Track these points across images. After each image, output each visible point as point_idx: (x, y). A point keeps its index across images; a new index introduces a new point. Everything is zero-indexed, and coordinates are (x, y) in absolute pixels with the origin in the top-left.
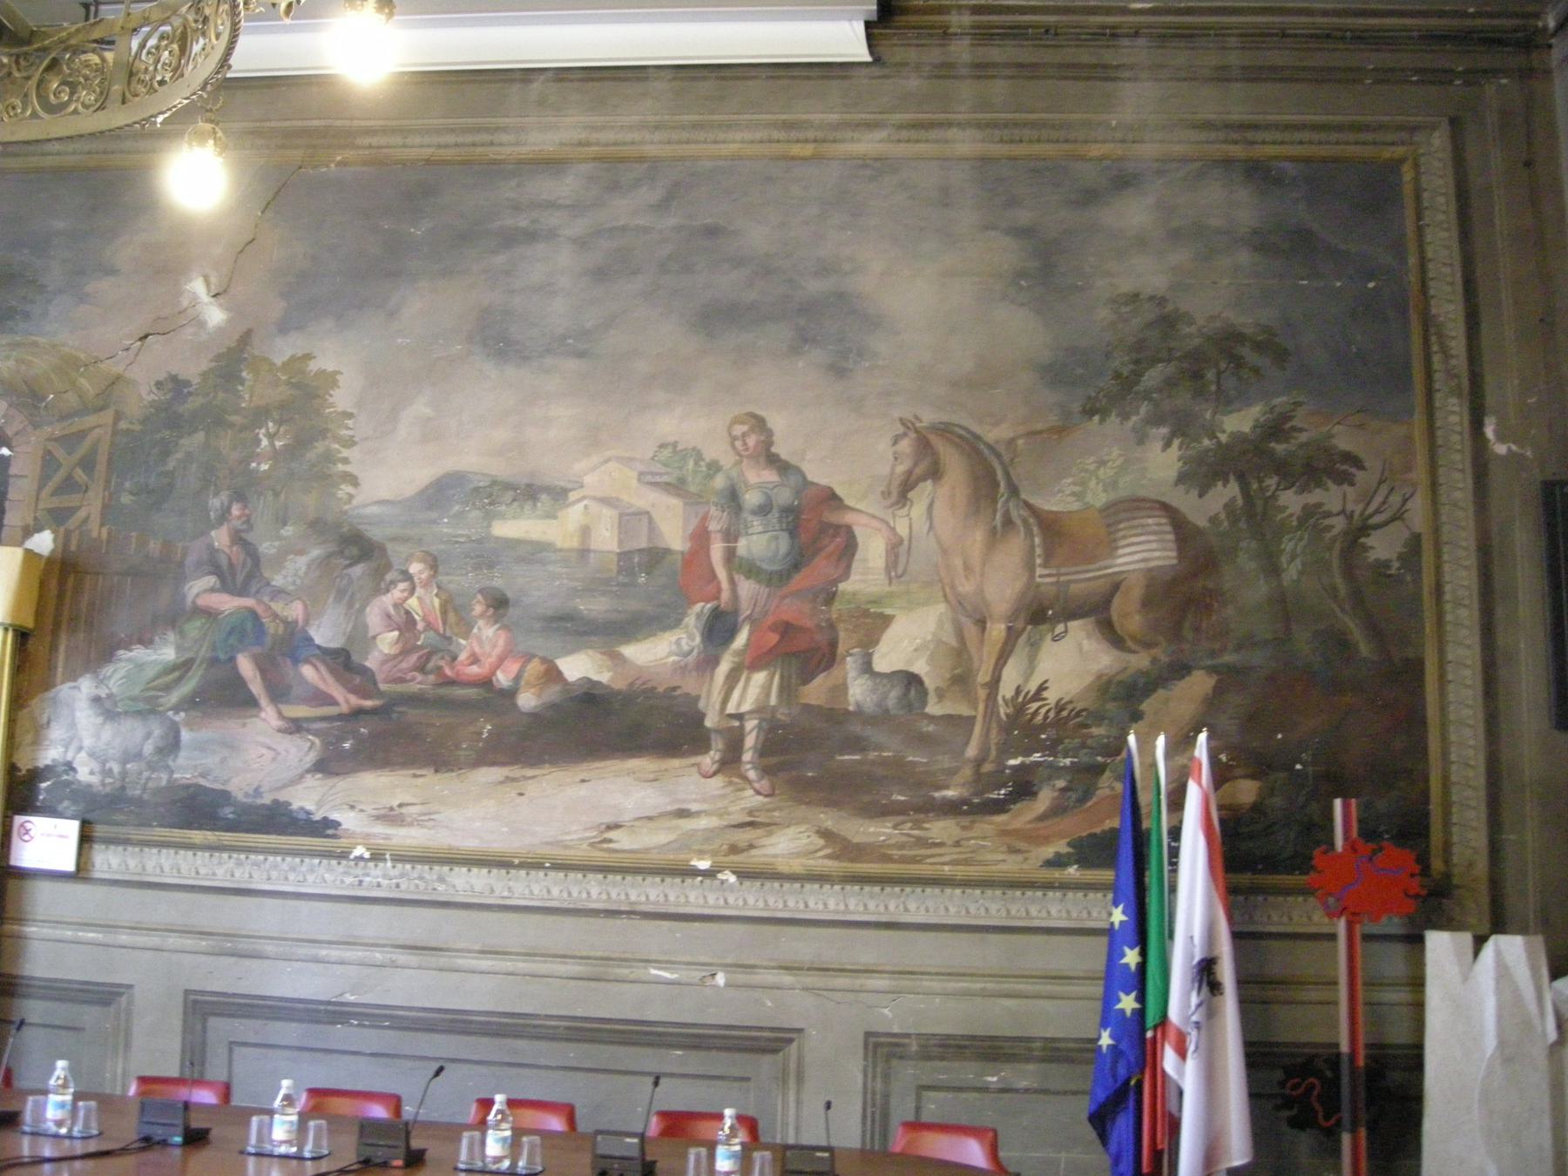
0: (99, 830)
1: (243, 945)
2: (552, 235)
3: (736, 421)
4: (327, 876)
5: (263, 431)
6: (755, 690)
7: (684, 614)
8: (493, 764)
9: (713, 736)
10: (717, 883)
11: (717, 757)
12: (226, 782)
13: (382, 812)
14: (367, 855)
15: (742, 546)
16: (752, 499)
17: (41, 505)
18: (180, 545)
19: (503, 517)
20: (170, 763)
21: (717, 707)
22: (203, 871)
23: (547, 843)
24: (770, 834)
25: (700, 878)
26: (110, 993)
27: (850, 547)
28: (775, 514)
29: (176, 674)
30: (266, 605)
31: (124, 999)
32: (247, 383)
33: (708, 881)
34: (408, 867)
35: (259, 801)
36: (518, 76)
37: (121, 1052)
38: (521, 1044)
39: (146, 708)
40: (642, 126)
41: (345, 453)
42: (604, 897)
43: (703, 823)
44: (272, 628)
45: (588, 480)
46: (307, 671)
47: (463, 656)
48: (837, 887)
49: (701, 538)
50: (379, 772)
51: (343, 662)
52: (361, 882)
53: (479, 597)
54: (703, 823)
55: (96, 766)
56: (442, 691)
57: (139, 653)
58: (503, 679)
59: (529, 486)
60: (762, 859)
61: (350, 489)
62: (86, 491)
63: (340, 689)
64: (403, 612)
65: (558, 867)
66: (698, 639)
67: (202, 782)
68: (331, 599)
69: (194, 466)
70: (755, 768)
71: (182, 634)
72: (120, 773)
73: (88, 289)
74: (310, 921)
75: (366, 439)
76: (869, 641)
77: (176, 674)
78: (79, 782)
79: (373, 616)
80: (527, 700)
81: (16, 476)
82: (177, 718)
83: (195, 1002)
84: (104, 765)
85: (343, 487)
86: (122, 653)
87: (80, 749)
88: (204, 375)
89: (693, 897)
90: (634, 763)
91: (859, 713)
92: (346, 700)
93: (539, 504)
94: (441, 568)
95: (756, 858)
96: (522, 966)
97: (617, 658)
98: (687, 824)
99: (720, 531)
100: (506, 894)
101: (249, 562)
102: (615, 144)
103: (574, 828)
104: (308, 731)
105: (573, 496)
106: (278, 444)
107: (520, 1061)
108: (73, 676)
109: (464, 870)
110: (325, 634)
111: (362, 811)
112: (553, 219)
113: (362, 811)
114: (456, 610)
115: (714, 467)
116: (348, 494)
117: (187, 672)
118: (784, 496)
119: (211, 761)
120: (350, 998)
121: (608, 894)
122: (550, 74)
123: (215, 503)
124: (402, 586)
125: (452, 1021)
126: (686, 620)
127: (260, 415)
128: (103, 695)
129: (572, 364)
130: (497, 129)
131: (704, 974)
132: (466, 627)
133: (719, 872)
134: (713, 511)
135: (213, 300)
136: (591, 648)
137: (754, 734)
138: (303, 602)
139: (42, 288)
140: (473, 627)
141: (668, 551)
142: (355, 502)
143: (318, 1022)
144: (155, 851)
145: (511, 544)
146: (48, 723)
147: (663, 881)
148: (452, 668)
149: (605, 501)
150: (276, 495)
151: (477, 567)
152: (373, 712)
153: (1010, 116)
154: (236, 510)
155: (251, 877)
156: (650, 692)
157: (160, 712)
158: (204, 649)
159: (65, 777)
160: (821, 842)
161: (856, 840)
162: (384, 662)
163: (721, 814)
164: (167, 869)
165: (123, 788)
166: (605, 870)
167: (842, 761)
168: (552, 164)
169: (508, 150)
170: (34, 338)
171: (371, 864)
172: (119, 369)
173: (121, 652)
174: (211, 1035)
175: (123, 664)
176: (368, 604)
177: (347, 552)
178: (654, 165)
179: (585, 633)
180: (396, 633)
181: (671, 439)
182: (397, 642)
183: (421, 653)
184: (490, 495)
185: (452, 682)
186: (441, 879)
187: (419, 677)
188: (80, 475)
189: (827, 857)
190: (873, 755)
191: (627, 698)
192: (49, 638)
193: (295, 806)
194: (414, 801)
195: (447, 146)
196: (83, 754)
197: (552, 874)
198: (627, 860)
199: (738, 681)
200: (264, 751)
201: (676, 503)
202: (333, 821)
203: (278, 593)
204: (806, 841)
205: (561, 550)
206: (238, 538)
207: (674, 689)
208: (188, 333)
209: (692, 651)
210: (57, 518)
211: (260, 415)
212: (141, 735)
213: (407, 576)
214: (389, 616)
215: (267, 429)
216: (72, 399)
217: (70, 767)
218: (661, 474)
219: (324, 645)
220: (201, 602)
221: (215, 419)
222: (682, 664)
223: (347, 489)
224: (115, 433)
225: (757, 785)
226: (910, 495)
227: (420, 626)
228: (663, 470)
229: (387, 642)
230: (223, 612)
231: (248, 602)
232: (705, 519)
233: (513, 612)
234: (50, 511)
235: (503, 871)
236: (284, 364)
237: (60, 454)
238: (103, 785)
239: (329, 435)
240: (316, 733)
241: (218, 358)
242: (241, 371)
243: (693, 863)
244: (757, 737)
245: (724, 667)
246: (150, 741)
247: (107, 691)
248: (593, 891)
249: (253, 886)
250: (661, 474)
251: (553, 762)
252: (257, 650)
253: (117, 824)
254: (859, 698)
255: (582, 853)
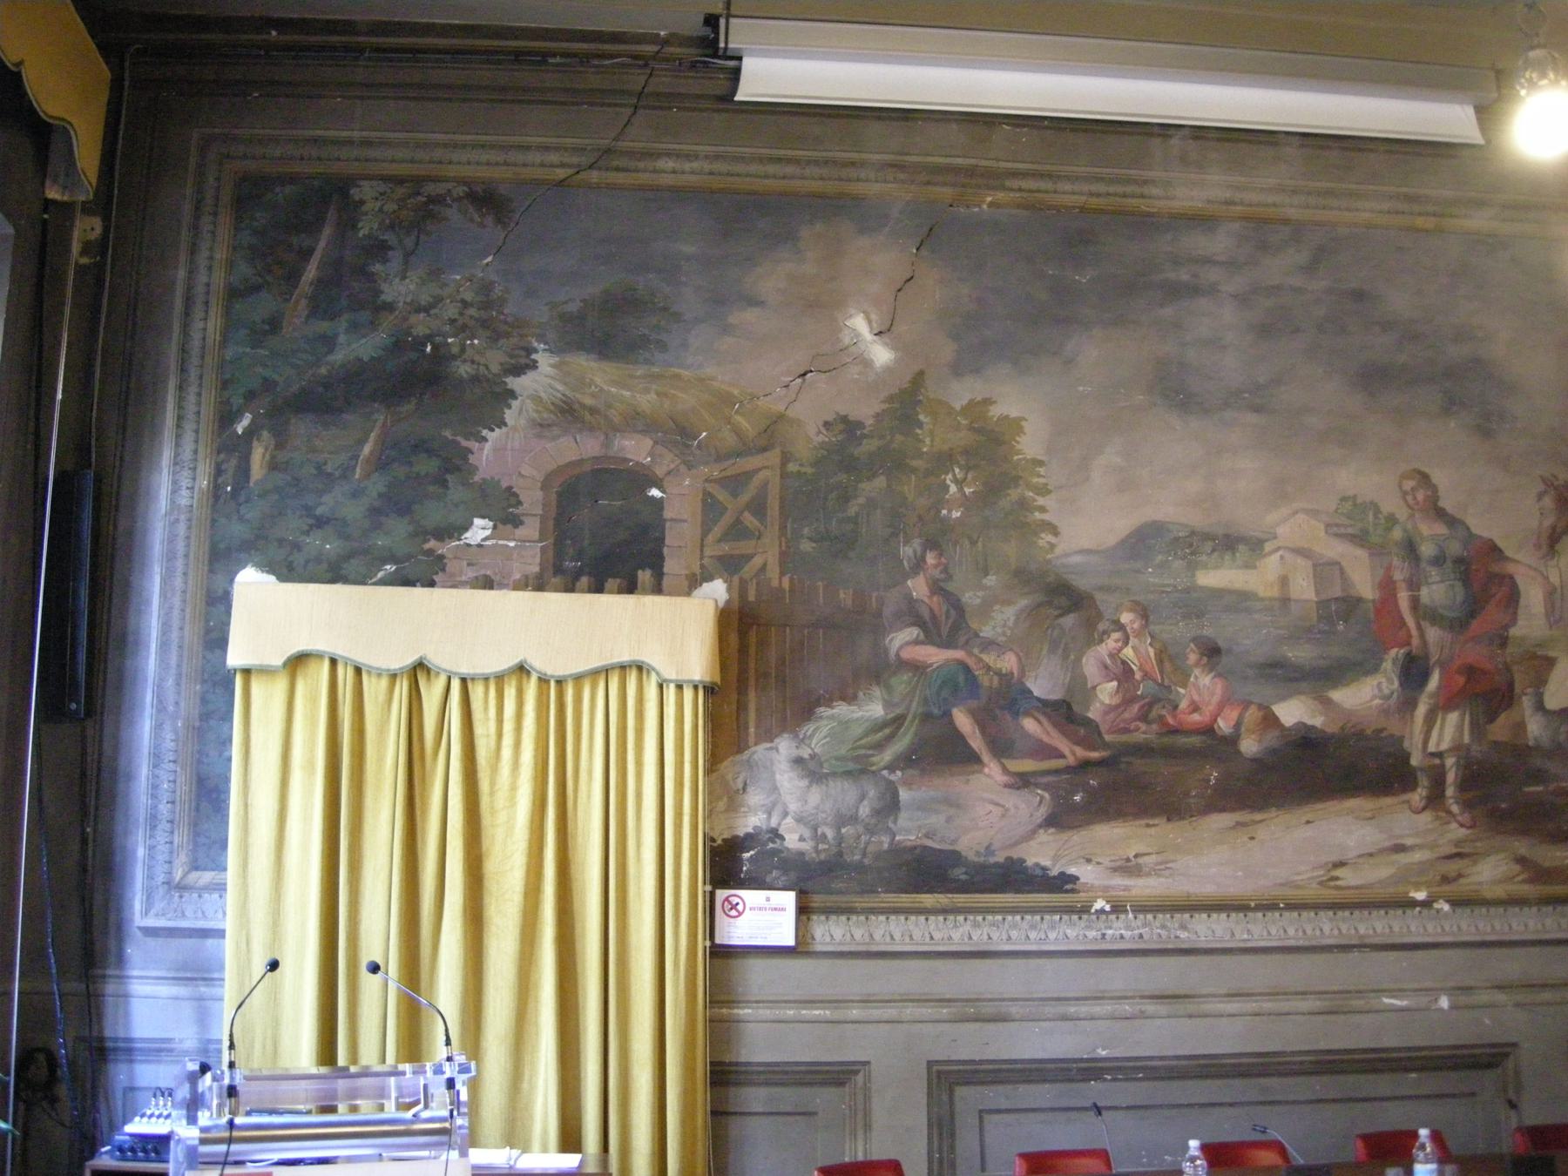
0: (817, 900)
1: (988, 1009)
2: (1212, 290)
3: (1404, 476)
4: (1069, 932)
5: (950, 476)
6: (1450, 730)
7: (1382, 660)
8: (1223, 810)
9: (1419, 773)
10: (1433, 912)
11: (1424, 794)
12: (954, 842)
13: (1118, 864)
14: (1108, 908)
15: (1424, 593)
16: (1427, 550)
17: (708, 552)
18: (874, 594)
19: (1205, 567)
20: (891, 825)
21: (1420, 746)
22: (937, 936)
23: (1281, 885)
24: (1475, 863)
25: (1418, 909)
26: (843, 1072)
27: (1513, 598)
28: (1449, 564)
29: (887, 731)
30: (976, 656)
31: (860, 1078)
32: (926, 427)
33: (1425, 912)
34: (1150, 916)
35: (992, 860)
36: (1156, 130)
37: (860, 1133)
38: (1273, 1082)
39: (858, 769)
40: (1281, 189)
41: (1041, 501)
42: (1336, 932)
43: (1417, 856)
44: (985, 680)
45: (1280, 531)
46: (1029, 724)
47: (1183, 705)
48: (1534, 909)
49: (1387, 586)
50: (1113, 824)
51: (1064, 713)
52: (1104, 935)
53: (1192, 645)
54: (1417, 856)
55: (807, 833)
56: (1166, 740)
57: (841, 709)
58: (1224, 726)
59: (1227, 536)
60: (1472, 887)
61: (1050, 538)
62: (759, 538)
63: (1065, 741)
64: (1119, 662)
65: (1292, 907)
66: (1396, 684)
67: (929, 843)
68: (1044, 652)
69: (879, 511)
70: (1457, 803)
71: (889, 688)
72: (834, 839)
73: (732, 320)
74: (1051, 978)
75: (1061, 487)
76: (1540, 682)
77: (887, 731)
78: (788, 849)
79: (1090, 666)
80: (1249, 746)
81: (672, 520)
82: (892, 777)
83: (939, 1072)
84: (816, 830)
85: (1043, 535)
86: (822, 711)
87: (785, 814)
88: (878, 417)
89: (1410, 927)
90: (1352, 803)
91: (1538, 748)
92: (1072, 753)
93: (1238, 555)
94: (1151, 617)
95: (1463, 887)
96: (1268, 1006)
97: (1327, 703)
98: (1404, 859)
99: (1404, 580)
100: (1245, 936)
101: (953, 612)
102: (1257, 205)
103: (1303, 868)
104: (1037, 785)
105: (1268, 547)
106: (967, 491)
107: (1271, 1098)
108: (768, 736)
109: (1204, 916)
110: (1042, 685)
111: (1098, 863)
112: (1212, 275)
113: (1098, 863)
114: (1171, 659)
115: (1392, 520)
116: (1048, 542)
117: (898, 728)
118: (1455, 548)
119: (936, 820)
120: (1103, 1053)
121: (1339, 930)
122: (1186, 132)
123: (907, 551)
124: (1116, 635)
125: (1206, 1066)
126: (1384, 664)
127: (944, 460)
128: (806, 756)
129: (1252, 418)
130: (1145, 182)
131: (1430, 998)
132: (1184, 679)
133: (1433, 902)
134: (1396, 562)
135: (875, 338)
136: (1300, 693)
137: (1454, 769)
138: (1017, 655)
139: (677, 317)
140: (1190, 676)
141: (1360, 600)
142: (1058, 551)
143: (1071, 1080)
144: (882, 918)
145: (1218, 593)
146: (744, 789)
147: (1386, 913)
148: (1174, 717)
149: (1299, 552)
150: (973, 543)
151: (1186, 616)
152: (1100, 763)
153: (768, 151)
154: (931, 559)
155: (990, 938)
156: (1360, 735)
157: (873, 772)
158: (914, 704)
159: (771, 845)
160: (1517, 868)
161: (1547, 864)
162: (1106, 713)
163: (1432, 846)
164: (897, 936)
165: (840, 854)
166: (1335, 906)
167: (1529, 793)
168: (1202, 221)
169: (1162, 203)
170: (677, 371)
171: (1113, 917)
172: (781, 408)
173: (822, 709)
174: (959, 1105)
175: (825, 722)
176: (1082, 656)
177: (1056, 602)
178: (1297, 230)
179: (1296, 680)
180: (1115, 684)
181: (1351, 493)
182: (1117, 692)
183: (1142, 702)
184: (1191, 545)
185: (1175, 731)
186: (1183, 927)
187: (1143, 727)
188: (750, 520)
189: (1523, 881)
190: (1552, 787)
191: (1341, 739)
192: (734, 697)
193: (1030, 862)
194: (1150, 850)
195: (1098, 195)
196: (789, 820)
197: (1287, 914)
198: (1351, 896)
199: (1435, 722)
200: (991, 807)
201: (1361, 553)
202: (1072, 876)
203: (988, 645)
204: (1505, 868)
205: (1262, 599)
206: (937, 588)
207: (1381, 730)
208: (854, 372)
209: (1392, 693)
210: (729, 566)
211: (944, 460)
212: (859, 799)
213: (1120, 627)
214: (1106, 667)
215: (954, 475)
216: (729, 439)
217: (775, 834)
218: (1346, 526)
219: (1043, 697)
220: (905, 655)
221: (893, 463)
222: (1385, 706)
223: (1047, 537)
224: (784, 475)
225: (1460, 818)
226: (1557, 547)
227: (1138, 676)
228: (1347, 522)
229: (1107, 692)
230: (931, 665)
231: (958, 654)
232: (1389, 569)
233: (1225, 660)
234: (720, 559)
235: (1241, 915)
236: (963, 408)
237: (722, 495)
238: (817, 851)
239: (1021, 482)
240: (1046, 787)
241: (890, 399)
242: (917, 415)
243: (1411, 895)
244: (1456, 775)
245: (1422, 710)
246: (865, 802)
247: (810, 751)
248: (1327, 928)
249: (992, 948)
250: (1346, 526)
251: (1279, 807)
252: (974, 704)
253: (840, 892)
254: (1536, 733)
255: (1312, 892)
